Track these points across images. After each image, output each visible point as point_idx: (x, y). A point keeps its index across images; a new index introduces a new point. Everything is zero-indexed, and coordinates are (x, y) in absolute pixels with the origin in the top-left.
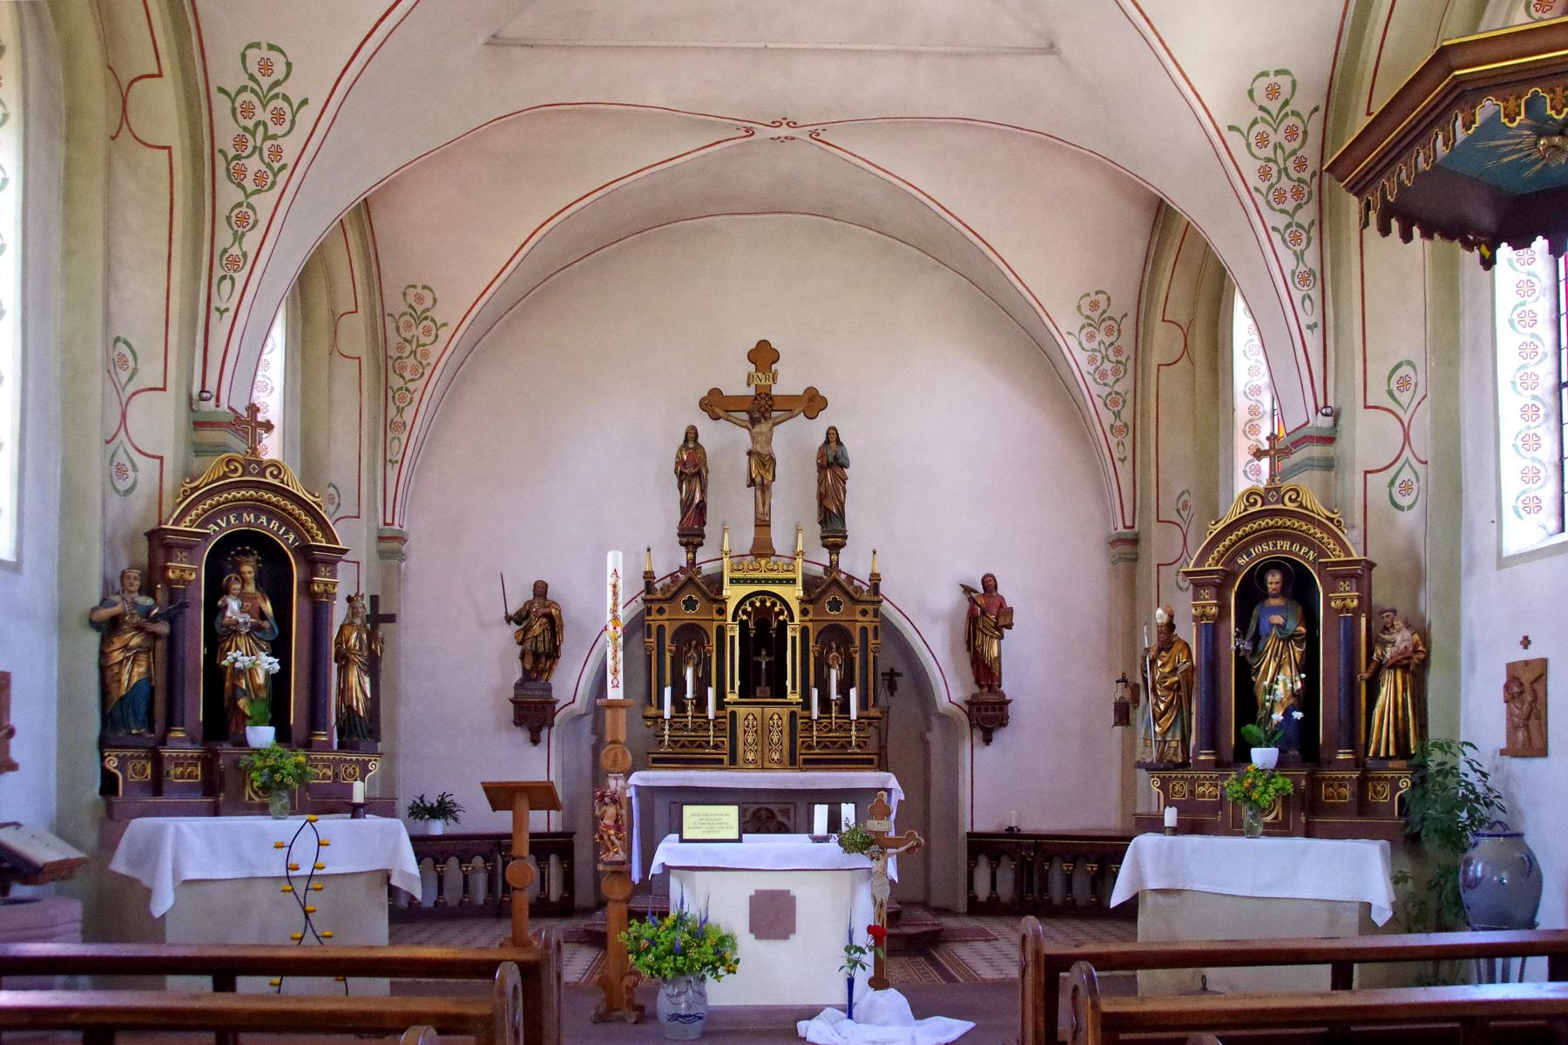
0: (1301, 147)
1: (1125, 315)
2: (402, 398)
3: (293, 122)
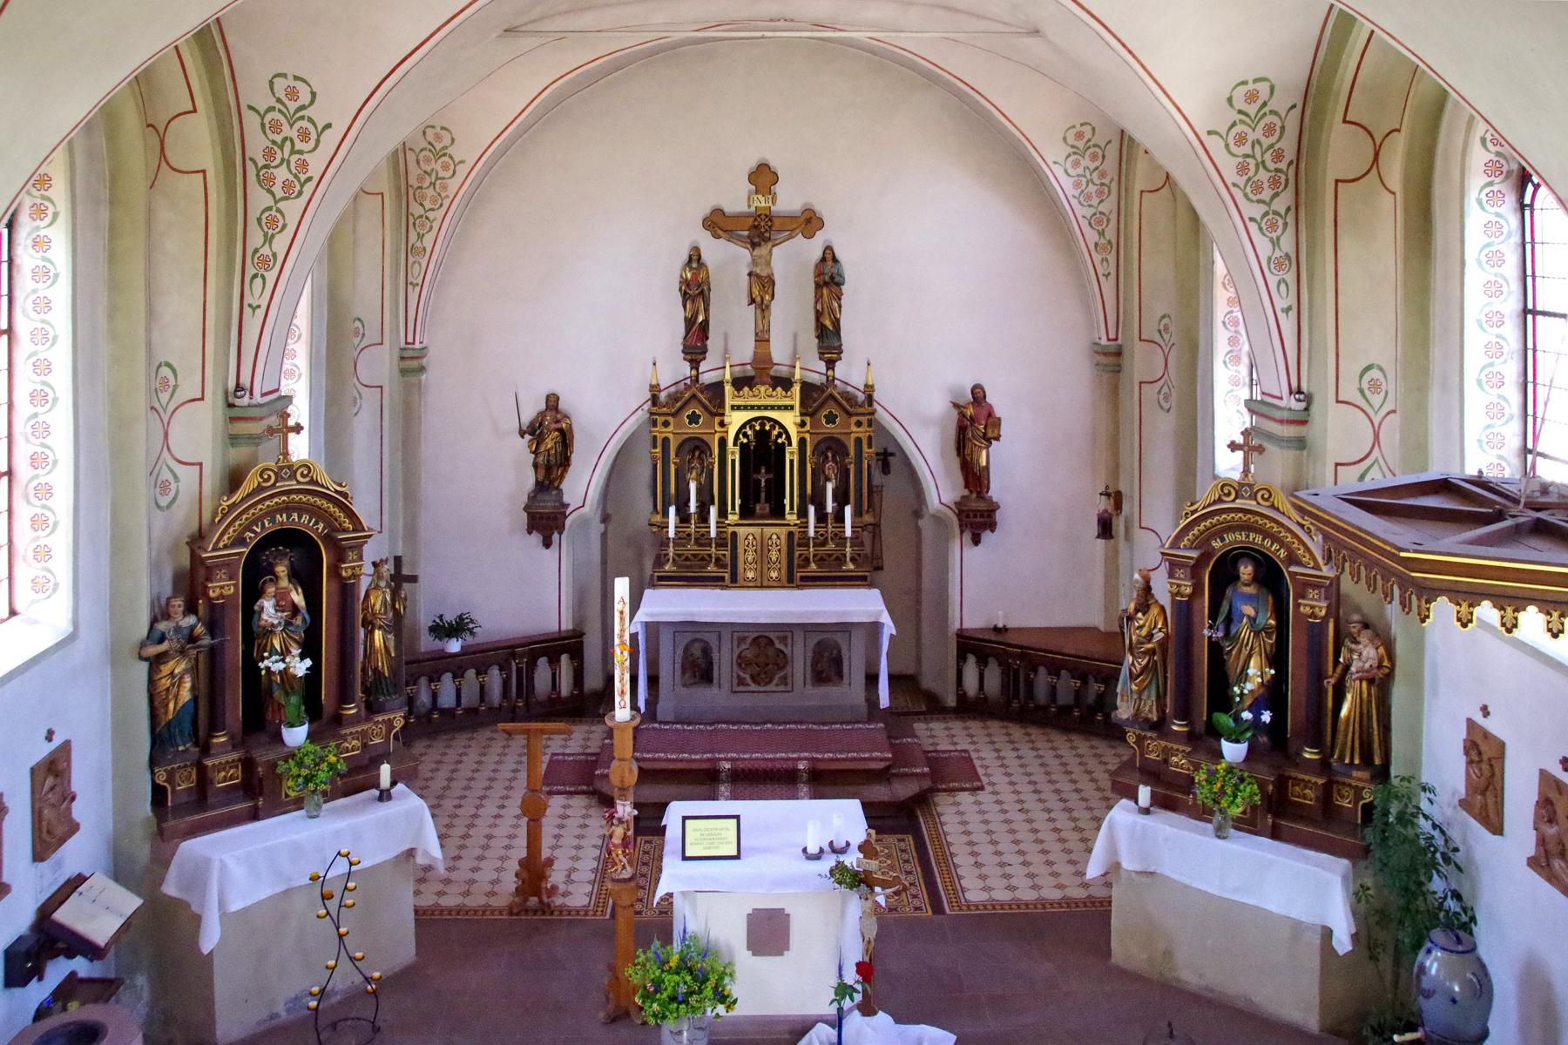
0: (1278, 140)
1: (1110, 142)
2: (423, 225)
3: (318, 141)
